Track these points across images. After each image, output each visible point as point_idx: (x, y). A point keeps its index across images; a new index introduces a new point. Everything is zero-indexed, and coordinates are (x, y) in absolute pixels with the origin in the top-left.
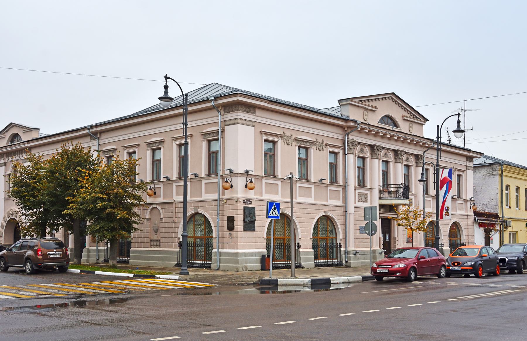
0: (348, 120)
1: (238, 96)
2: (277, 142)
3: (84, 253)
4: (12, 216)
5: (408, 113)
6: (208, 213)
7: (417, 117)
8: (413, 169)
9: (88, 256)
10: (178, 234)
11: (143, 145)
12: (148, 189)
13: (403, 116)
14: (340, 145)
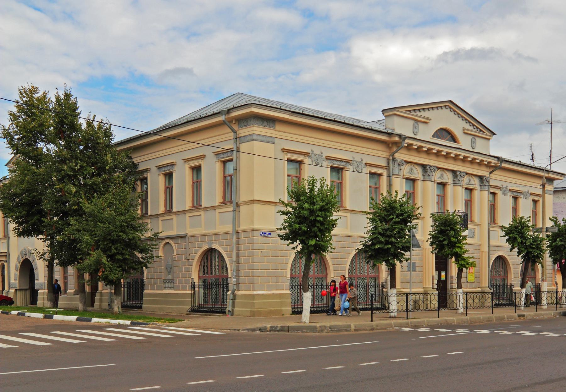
0: (392, 134)
1: (252, 107)
2: (538, 201)
3: (97, 298)
4: (26, 256)
5: (470, 126)
6: (222, 248)
7: (481, 130)
8: (476, 193)
9: (101, 301)
10: (191, 273)
11: (154, 169)
12: (116, 216)
13: (464, 129)
14: (383, 163)
